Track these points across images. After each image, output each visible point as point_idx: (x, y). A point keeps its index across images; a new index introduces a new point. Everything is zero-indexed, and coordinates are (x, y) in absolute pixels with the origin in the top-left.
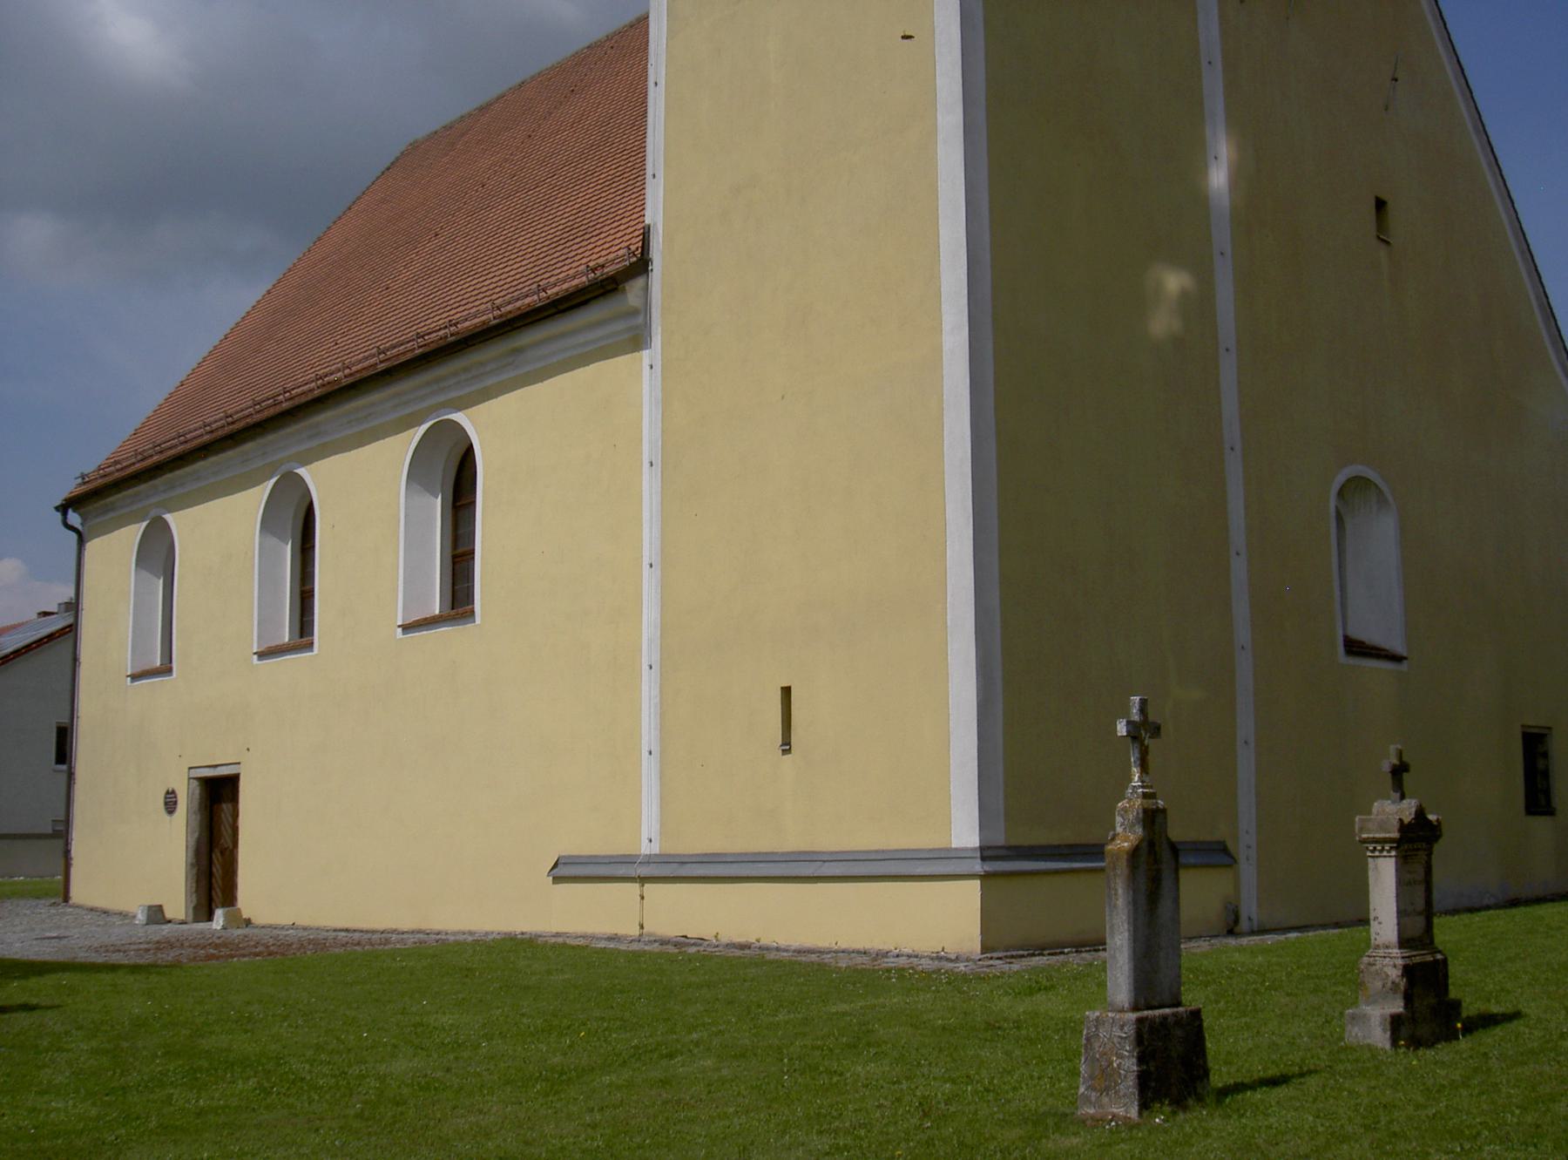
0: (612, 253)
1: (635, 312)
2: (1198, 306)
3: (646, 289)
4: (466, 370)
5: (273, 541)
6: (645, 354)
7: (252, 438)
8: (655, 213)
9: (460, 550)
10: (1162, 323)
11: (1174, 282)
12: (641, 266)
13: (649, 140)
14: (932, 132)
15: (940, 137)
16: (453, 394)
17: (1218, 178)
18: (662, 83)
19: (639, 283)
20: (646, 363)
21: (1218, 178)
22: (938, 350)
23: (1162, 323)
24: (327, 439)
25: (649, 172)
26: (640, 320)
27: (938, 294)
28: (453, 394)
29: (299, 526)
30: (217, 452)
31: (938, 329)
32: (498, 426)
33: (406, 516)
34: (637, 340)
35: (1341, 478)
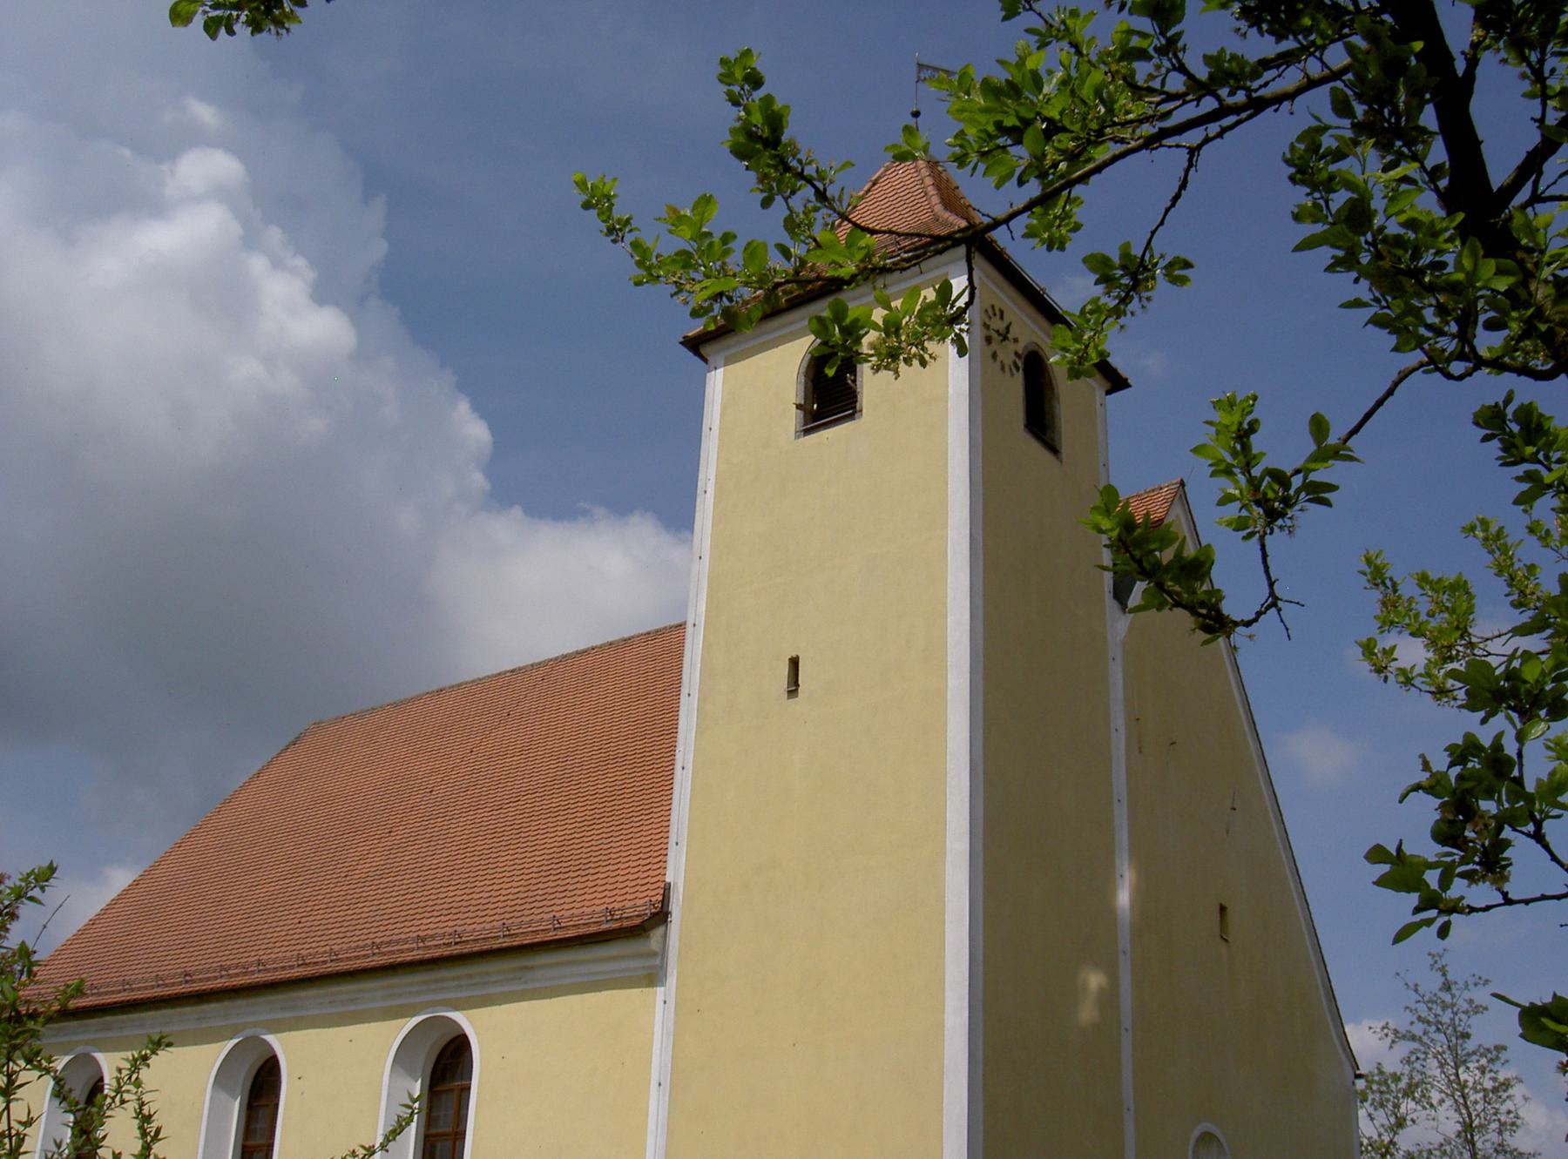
0: (636, 904)
1: (654, 954)
2: (1108, 999)
3: (665, 936)
4: (470, 976)
5: (224, 1096)
6: (660, 991)
7: (218, 1001)
8: (676, 872)
9: (433, 1131)
10: (1087, 1013)
11: (1095, 980)
12: (661, 916)
13: (674, 813)
14: (941, 854)
15: (949, 858)
16: (451, 995)
17: (1124, 898)
18: (690, 767)
19: (661, 930)
20: (659, 1002)
21: (1124, 898)
22: (940, 1025)
23: (1087, 1013)
24: (304, 1013)
25: (673, 839)
26: (658, 961)
27: (942, 981)
28: (451, 995)
29: (262, 1087)
30: (173, 1007)
31: (941, 1009)
32: (496, 1032)
33: (389, 1095)
34: (653, 977)
35: (1196, 1133)
